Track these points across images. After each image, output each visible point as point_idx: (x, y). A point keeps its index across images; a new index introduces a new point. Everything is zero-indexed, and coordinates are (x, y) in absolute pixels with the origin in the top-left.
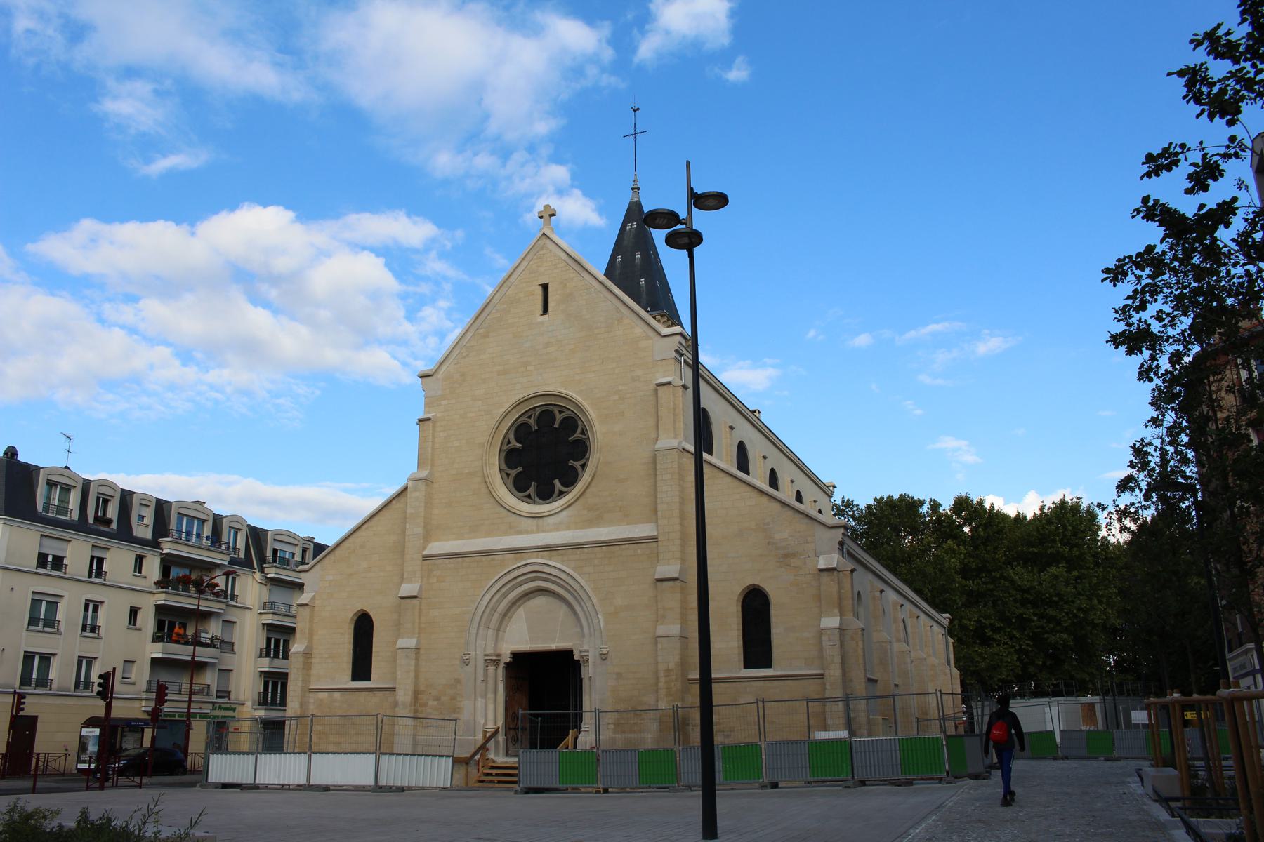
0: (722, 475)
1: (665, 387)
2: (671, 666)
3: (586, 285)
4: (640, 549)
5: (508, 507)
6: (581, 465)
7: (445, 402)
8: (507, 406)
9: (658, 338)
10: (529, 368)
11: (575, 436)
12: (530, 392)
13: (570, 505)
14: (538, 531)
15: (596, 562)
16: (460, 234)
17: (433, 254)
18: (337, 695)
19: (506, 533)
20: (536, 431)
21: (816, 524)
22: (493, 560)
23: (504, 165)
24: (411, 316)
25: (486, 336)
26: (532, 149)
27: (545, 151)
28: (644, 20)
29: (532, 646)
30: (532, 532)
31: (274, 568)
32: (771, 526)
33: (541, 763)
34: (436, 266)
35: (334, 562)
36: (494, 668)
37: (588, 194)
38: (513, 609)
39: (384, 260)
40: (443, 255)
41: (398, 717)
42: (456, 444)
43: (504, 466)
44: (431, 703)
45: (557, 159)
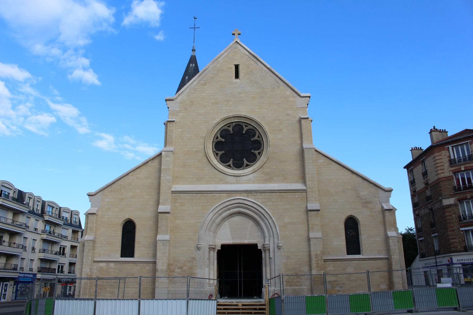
0: (334, 163)
1: (305, 120)
2: (318, 252)
3: (260, 68)
4: (297, 195)
5: (220, 170)
6: (258, 153)
7: (180, 114)
8: (218, 120)
9: (298, 97)
10: (230, 103)
11: (254, 138)
12: (231, 114)
13: (255, 171)
14: (237, 183)
15: (273, 200)
16: (40, 78)
17: (28, 84)
18: (112, 265)
19: (218, 183)
20: (243, 133)
21: (379, 189)
22: (214, 196)
23: (63, 54)
24: (14, 107)
25: (205, 84)
26: (76, 50)
27: (81, 52)
28: (128, 10)
29: (233, 241)
30: (234, 183)
31: (2, 199)
32: (358, 188)
33: (296, 303)
34: (27, 89)
35: (111, 191)
36: (213, 252)
37: (95, 71)
38: (223, 221)
39: (4, 83)
40: (32, 86)
41: (159, 277)
42: (188, 136)
43: (215, 150)
44: (177, 270)
45: (85, 56)
